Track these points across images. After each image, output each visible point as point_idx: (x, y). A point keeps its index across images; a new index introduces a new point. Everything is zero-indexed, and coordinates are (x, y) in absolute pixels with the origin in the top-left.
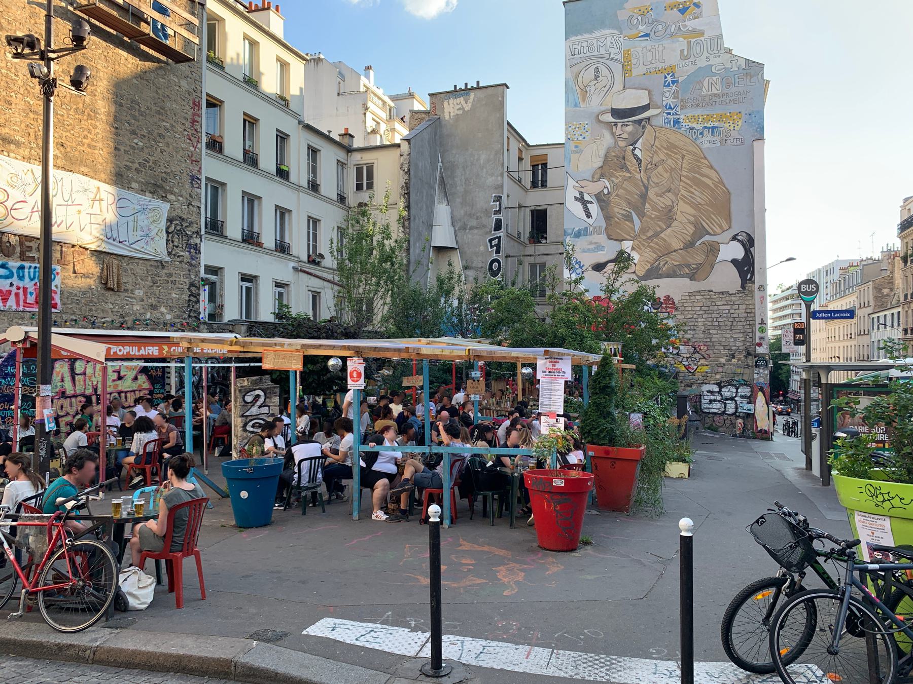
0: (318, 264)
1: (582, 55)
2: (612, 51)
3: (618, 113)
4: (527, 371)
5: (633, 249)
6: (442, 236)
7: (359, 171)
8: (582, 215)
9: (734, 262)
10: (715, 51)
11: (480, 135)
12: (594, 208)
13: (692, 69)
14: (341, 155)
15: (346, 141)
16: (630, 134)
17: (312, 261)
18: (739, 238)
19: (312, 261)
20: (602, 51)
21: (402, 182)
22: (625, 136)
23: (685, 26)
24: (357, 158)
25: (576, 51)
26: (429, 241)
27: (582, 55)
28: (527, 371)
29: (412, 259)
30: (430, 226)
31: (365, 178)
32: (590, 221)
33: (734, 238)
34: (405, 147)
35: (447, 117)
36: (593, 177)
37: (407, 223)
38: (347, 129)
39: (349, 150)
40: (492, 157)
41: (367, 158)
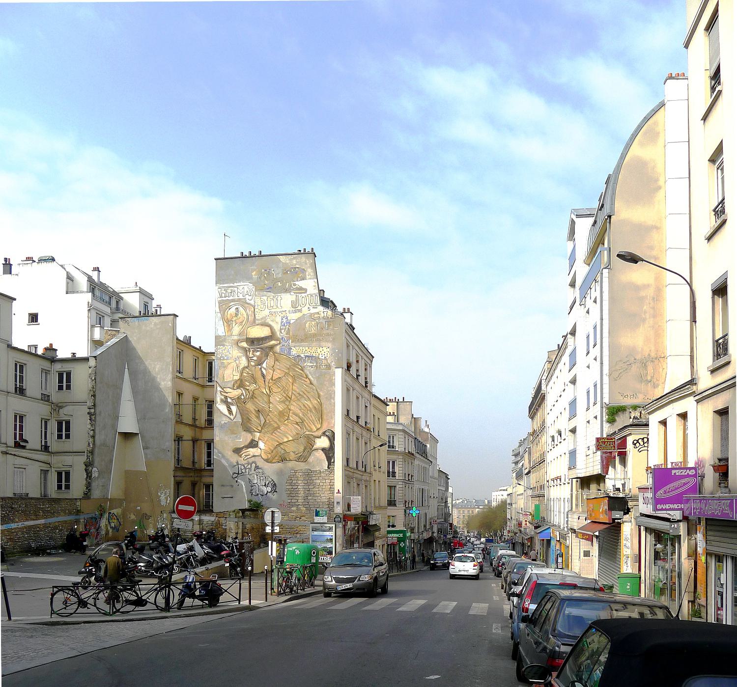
0: (24, 447)
1: (227, 298)
2: (247, 297)
3: (252, 341)
4: (674, 465)
5: (259, 439)
6: (128, 422)
7: (61, 375)
8: (226, 412)
9: (323, 450)
10: (314, 304)
11: (156, 350)
12: (234, 409)
13: (299, 315)
14: (46, 365)
15: (49, 354)
16: (258, 357)
17: (17, 445)
18: (327, 434)
19: (17, 445)
20: (241, 297)
21: (90, 386)
22: (255, 358)
23: (295, 285)
24: (58, 367)
25: (223, 295)
26: (114, 426)
27: (227, 298)
28: (674, 465)
29: (98, 442)
30: (116, 418)
31: (65, 381)
32: (232, 417)
33: (324, 434)
34: (92, 362)
35: (440, 81)
36: (234, 386)
37: (93, 417)
38: (51, 345)
39: (53, 360)
40: (164, 367)
41: (66, 367)
